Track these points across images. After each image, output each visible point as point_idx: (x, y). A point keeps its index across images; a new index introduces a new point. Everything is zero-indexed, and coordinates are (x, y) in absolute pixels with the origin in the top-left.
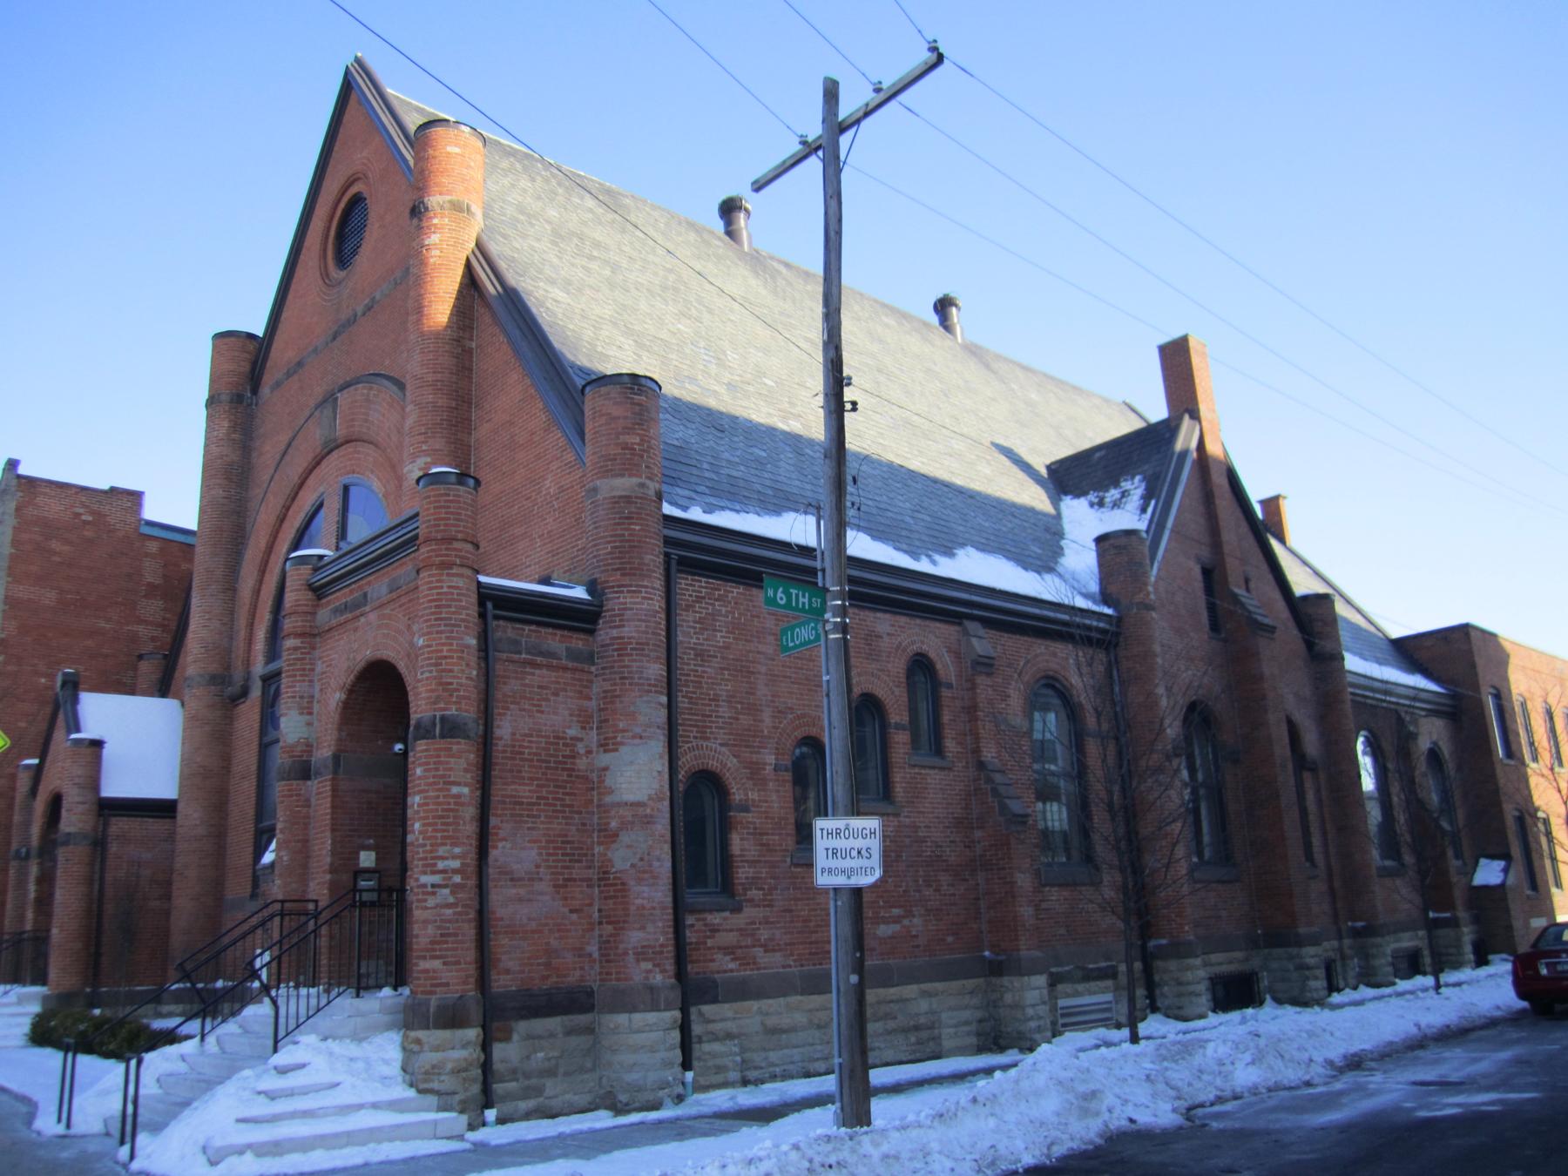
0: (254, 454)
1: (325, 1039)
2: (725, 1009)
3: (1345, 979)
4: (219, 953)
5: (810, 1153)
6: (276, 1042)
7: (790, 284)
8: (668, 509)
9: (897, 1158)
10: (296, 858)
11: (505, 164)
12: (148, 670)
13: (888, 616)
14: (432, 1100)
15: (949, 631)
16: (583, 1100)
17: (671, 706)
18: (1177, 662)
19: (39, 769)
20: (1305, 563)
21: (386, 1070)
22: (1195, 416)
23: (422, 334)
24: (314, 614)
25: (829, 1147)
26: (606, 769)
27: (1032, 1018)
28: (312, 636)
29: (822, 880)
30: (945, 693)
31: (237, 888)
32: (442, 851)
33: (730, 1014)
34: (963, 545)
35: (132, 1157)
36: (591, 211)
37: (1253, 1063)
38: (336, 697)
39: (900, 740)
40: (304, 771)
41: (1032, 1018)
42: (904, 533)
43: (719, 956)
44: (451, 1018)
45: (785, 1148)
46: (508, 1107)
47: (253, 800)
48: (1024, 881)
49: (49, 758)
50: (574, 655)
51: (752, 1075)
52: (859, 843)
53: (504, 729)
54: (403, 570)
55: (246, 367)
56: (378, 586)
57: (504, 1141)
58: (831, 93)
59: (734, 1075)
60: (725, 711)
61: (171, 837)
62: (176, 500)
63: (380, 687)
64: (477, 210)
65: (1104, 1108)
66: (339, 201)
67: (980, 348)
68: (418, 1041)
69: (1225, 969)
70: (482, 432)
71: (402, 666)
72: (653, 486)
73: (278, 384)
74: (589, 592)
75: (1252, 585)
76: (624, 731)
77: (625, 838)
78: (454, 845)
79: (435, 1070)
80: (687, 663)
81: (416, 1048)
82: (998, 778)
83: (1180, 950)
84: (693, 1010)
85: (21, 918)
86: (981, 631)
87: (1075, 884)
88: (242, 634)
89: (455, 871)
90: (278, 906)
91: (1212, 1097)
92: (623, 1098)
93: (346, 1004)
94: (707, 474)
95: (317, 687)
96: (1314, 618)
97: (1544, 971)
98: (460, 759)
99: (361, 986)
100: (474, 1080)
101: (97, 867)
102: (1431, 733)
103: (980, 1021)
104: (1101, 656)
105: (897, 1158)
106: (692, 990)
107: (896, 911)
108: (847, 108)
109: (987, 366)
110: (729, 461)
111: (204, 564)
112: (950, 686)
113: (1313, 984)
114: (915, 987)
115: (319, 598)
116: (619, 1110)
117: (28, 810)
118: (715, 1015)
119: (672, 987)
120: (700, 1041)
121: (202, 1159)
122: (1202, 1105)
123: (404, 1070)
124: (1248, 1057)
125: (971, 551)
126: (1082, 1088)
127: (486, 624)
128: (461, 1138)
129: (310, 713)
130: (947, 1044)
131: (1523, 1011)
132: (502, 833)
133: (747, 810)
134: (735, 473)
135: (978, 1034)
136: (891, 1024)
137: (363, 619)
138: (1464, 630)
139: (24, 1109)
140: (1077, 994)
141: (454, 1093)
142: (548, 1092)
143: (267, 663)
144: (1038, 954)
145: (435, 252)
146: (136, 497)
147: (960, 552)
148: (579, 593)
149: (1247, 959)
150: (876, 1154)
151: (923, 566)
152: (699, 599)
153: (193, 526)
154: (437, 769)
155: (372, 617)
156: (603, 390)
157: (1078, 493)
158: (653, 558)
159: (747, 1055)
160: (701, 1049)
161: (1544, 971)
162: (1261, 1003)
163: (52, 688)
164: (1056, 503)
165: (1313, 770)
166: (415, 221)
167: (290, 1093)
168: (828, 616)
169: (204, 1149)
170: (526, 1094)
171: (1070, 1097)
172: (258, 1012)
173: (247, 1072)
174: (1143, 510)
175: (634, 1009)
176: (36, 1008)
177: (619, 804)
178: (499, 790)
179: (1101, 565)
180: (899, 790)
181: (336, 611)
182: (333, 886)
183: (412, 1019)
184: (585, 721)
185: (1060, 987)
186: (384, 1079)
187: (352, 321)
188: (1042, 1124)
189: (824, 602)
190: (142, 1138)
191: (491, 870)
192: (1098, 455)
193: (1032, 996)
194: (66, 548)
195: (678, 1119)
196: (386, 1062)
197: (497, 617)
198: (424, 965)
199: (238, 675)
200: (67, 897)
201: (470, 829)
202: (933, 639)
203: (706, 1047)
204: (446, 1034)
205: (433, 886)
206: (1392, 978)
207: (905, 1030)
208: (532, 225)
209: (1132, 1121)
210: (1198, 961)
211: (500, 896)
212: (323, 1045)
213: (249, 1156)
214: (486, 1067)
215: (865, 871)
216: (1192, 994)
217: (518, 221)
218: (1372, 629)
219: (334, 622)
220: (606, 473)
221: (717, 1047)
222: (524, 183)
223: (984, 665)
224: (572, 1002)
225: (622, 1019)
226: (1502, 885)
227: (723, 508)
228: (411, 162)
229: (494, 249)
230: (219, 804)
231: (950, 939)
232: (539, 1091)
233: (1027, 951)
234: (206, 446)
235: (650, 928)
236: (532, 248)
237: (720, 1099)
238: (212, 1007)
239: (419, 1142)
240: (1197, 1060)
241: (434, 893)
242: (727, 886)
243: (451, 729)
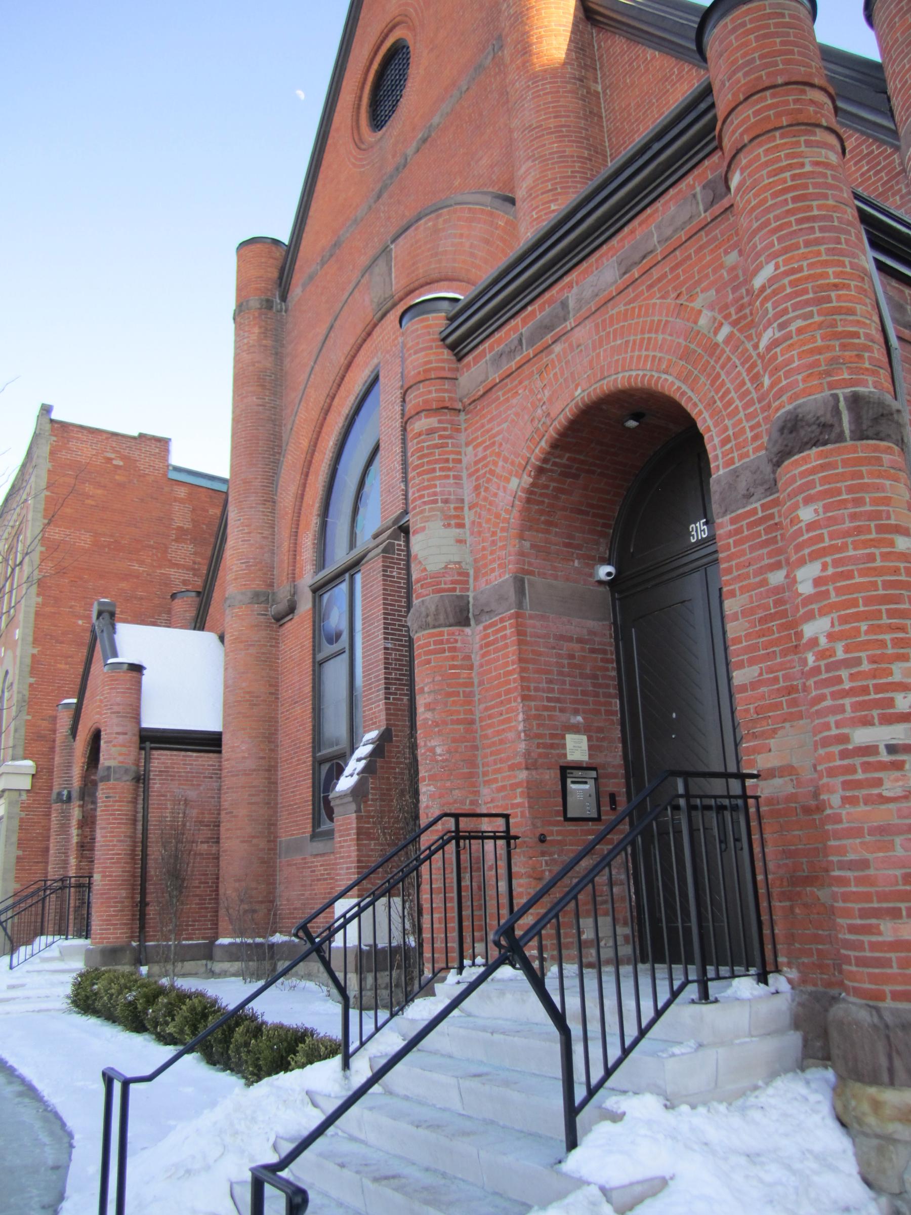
6: (572, 1111)
12: (184, 606)
47: (309, 726)
55: (276, 274)
61: (217, 774)
62: (205, 445)
101: (140, 806)
117: (69, 751)
129: (461, 526)
137: (558, 348)
143: (316, 573)
146: (163, 444)
154: (859, 502)
155: (580, 334)
176: (79, 965)
194: (99, 492)
199: (283, 593)
200: (111, 841)
205: (892, 749)
212: (669, 1117)
241: (898, 766)
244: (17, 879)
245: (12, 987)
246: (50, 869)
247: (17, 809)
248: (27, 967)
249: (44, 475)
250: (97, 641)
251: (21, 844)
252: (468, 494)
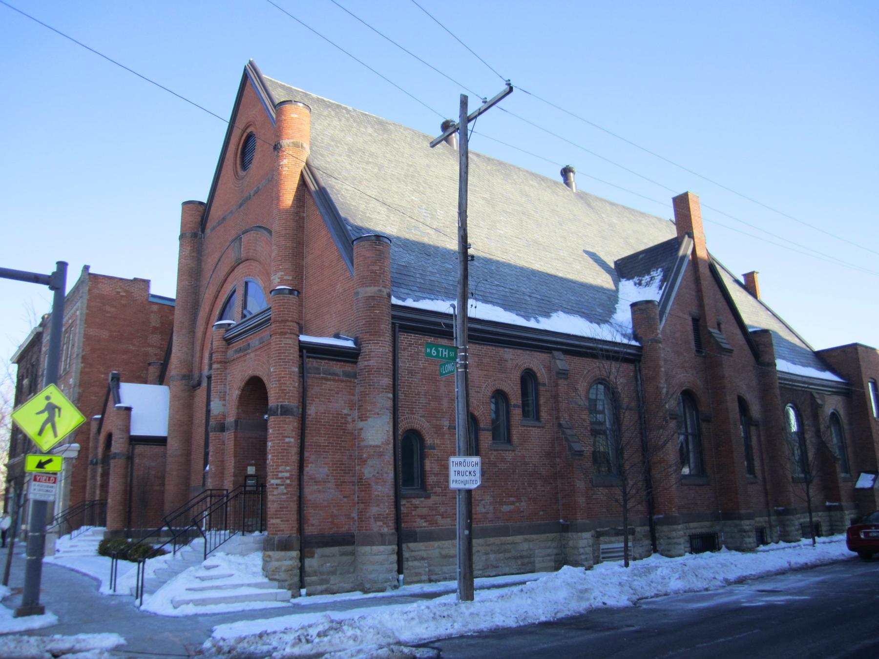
0: (203, 263)
1: (228, 554)
2: (421, 545)
3: (771, 538)
4: (186, 511)
5: (435, 610)
6: (205, 555)
7: (478, 166)
8: (394, 301)
9: (478, 615)
10: (220, 470)
11: (326, 113)
12: (153, 371)
13: (511, 350)
14: (276, 583)
15: (544, 356)
16: (347, 586)
17: (395, 400)
18: (675, 369)
19: (101, 421)
20: (768, 309)
21: (255, 569)
22: (691, 236)
23: (280, 210)
24: (226, 352)
25: (444, 608)
26: (361, 429)
27: (582, 554)
28: (225, 363)
29: (453, 486)
30: (542, 388)
31: (196, 481)
32: (281, 468)
33: (423, 548)
34: (556, 311)
35: (141, 604)
36: (370, 135)
37: (680, 578)
38: (237, 393)
39: (517, 413)
40: (222, 428)
41: (582, 554)
42: (524, 306)
43: (418, 520)
44: (284, 546)
45: (423, 607)
46: (312, 588)
47: (203, 437)
48: (580, 484)
49: (106, 415)
50: (347, 374)
51: (434, 577)
52: (470, 468)
53: (312, 410)
54: (265, 333)
55: (200, 219)
56: (254, 341)
57: (308, 603)
58: (464, 102)
59: (425, 577)
60: (423, 400)
61: (164, 455)
62: (165, 284)
63: (255, 388)
64: (307, 146)
65: (592, 597)
67: (586, 194)
68: (269, 556)
69: (699, 531)
70: (309, 259)
71: (265, 379)
72: (385, 291)
73: (214, 228)
74: (355, 343)
75: (722, 326)
76: (370, 411)
77: (370, 462)
78: (287, 465)
79: (277, 570)
80: (403, 375)
81: (268, 559)
82: (569, 432)
83: (670, 521)
84: (404, 546)
85: (94, 493)
86: (562, 356)
87: (612, 486)
88: (198, 354)
89: (287, 478)
90: (209, 492)
91: (652, 594)
92: (367, 586)
93: (238, 538)
94: (418, 280)
95: (228, 387)
96: (760, 344)
97: (862, 536)
98: (290, 425)
99: (246, 529)
100: (295, 575)
102: (832, 405)
103: (556, 555)
104: (631, 367)
105: (478, 615)
106: (403, 536)
107: (512, 499)
108: (471, 110)
109: (589, 205)
110: (431, 272)
111: (179, 317)
112: (544, 385)
113: (747, 540)
114: (521, 537)
115: (229, 344)
116: (366, 592)
117: (96, 440)
118: (414, 549)
119: (392, 534)
120: (408, 561)
121: (171, 606)
122: (647, 598)
123: (263, 569)
124: (677, 575)
125: (560, 313)
126: (580, 587)
127: (303, 360)
128: (288, 601)
130: (537, 566)
131: (855, 557)
132: (310, 460)
133: (434, 449)
134: (433, 279)
135: (555, 561)
136: (508, 555)
138: (854, 347)
139: (95, 583)
140: (611, 542)
141: (286, 581)
142: (332, 582)
144: (587, 521)
145: (285, 169)
146: (146, 283)
147: (554, 315)
148: (350, 344)
149: (711, 527)
150: (467, 612)
151: (532, 324)
152: (411, 345)
153: (174, 297)
155: (252, 355)
156: (363, 243)
157: (629, 278)
158: (386, 327)
159: (432, 568)
160: (406, 565)
161: (862, 536)
162: (719, 549)
163: (107, 380)
164: (616, 283)
165: (757, 425)
167: (211, 578)
168: (458, 360)
169: (172, 602)
170: (321, 582)
171: (574, 591)
172: (199, 541)
173: (192, 568)
174: (660, 288)
175: (373, 544)
176: (101, 538)
177: (366, 446)
178: (309, 440)
179: (633, 319)
180: (515, 439)
181: (236, 351)
182: (235, 483)
183: (267, 546)
184: (352, 406)
185: (602, 538)
186: (254, 574)
187: (249, 198)
188: (556, 603)
189: (456, 354)
190: (145, 596)
191: (305, 477)
192: (641, 256)
193: (582, 543)
194: (113, 309)
195: (392, 596)
196: (255, 566)
197: (308, 357)
198: (272, 521)
200: (115, 484)
201: (294, 458)
202: (535, 361)
203: (410, 563)
204: (283, 553)
206: (798, 538)
207: (516, 558)
208: (338, 147)
209: (604, 603)
210: (680, 527)
211: (310, 491)
212: (227, 557)
213: (191, 605)
214: (302, 569)
215: (472, 481)
217: (330, 145)
218: (804, 346)
219: (235, 357)
220: (363, 285)
221: (416, 563)
222: (336, 123)
223: (563, 374)
224: (344, 540)
225: (367, 549)
226: (872, 488)
227: (424, 298)
228: (274, 116)
229: (315, 163)
230: (187, 439)
231: (541, 513)
232: (327, 581)
233: (580, 521)
234: (179, 259)
235: (382, 506)
236: (337, 161)
237: (416, 588)
238: (182, 538)
239: (268, 603)
240: (652, 576)
242: (423, 486)
243: (285, 411)
244: (71, 500)
245: (72, 546)
246: (87, 495)
247: (71, 467)
248: (78, 538)
249: (85, 302)
250: (111, 391)
251: (72, 484)
252: (228, 391)
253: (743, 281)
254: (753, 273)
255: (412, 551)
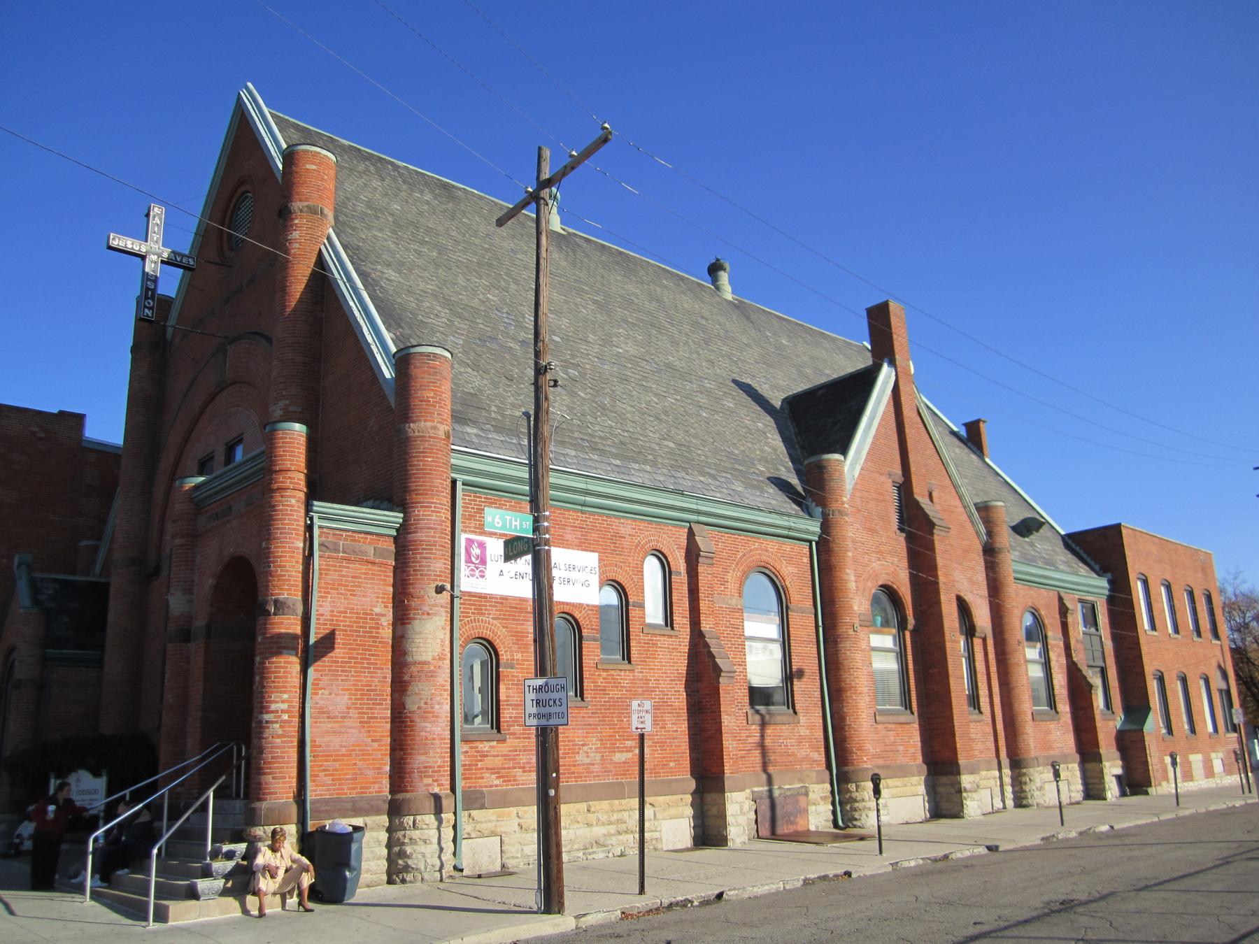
11: (361, 167)
36: (428, 203)
38: (210, 581)
40: (185, 635)
62: (107, 425)
66: (232, 197)
109: (748, 318)
129: (192, 594)
146: (79, 419)
166: (281, 221)
192: (821, 392)
216: (865, 808)
222: (376, 183)
236: (376, 237)
253: (963, 433)
254: (978, 421)
255: (478, 822)
